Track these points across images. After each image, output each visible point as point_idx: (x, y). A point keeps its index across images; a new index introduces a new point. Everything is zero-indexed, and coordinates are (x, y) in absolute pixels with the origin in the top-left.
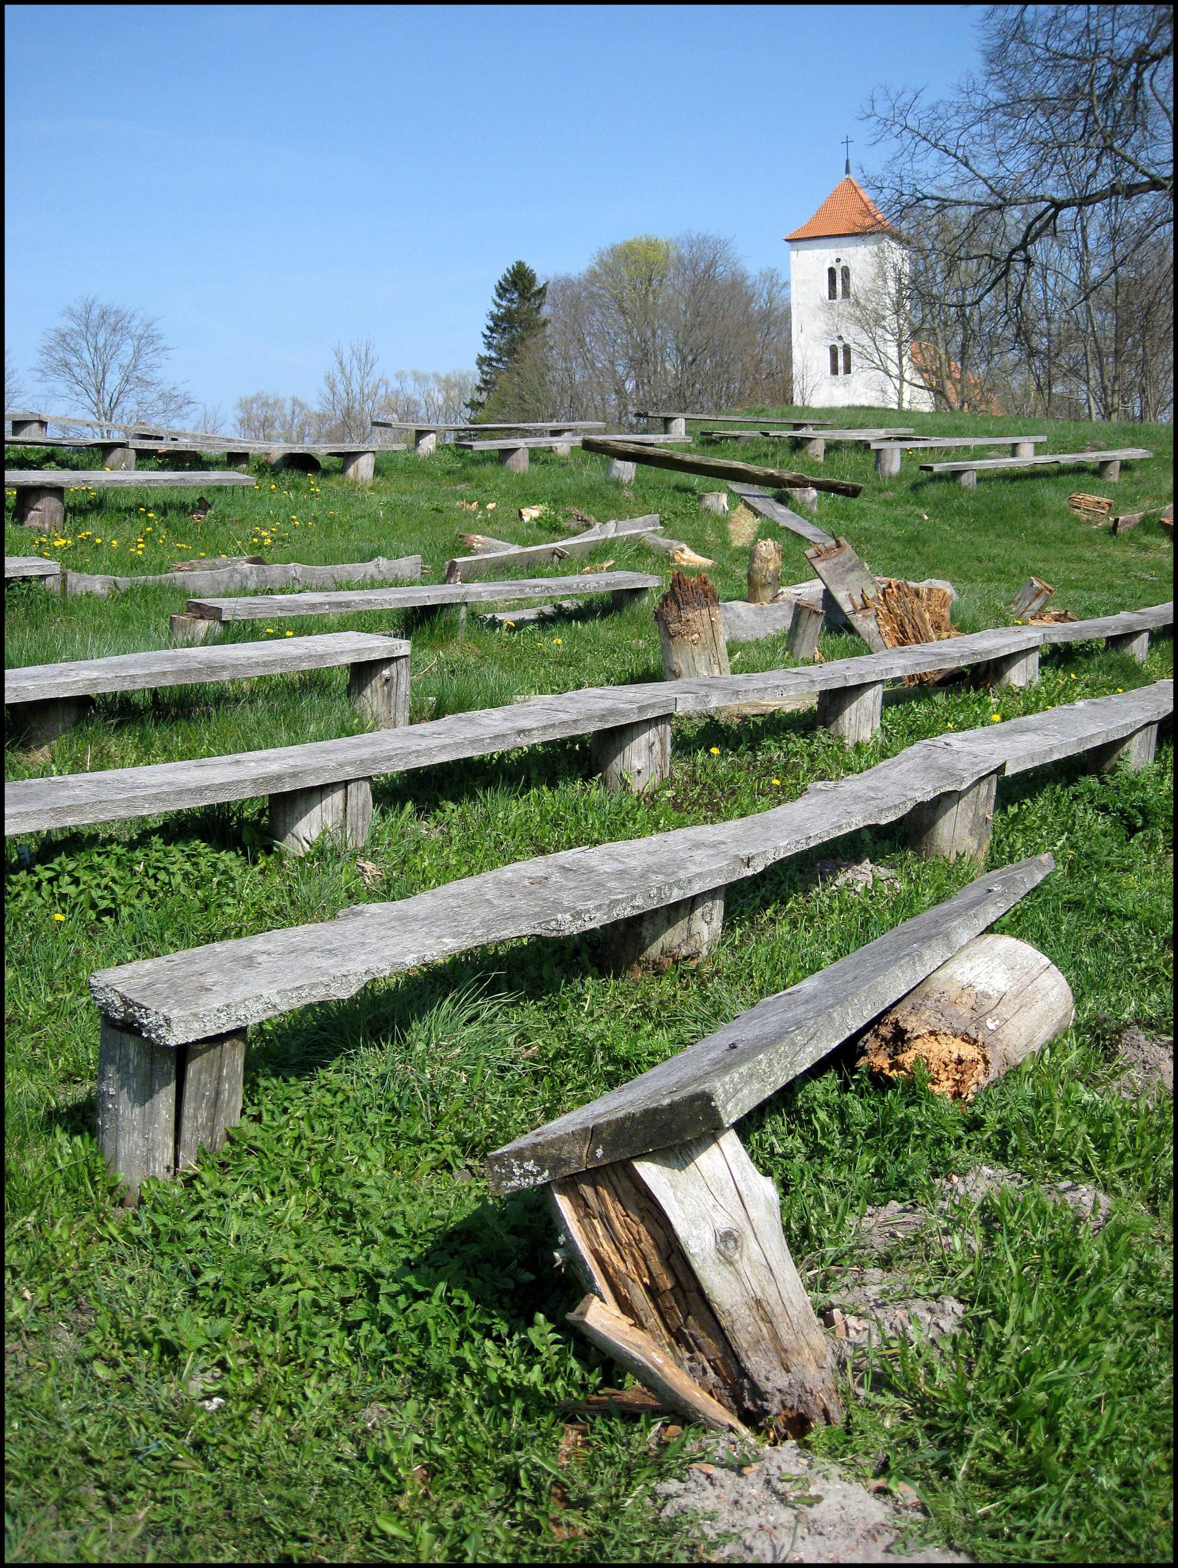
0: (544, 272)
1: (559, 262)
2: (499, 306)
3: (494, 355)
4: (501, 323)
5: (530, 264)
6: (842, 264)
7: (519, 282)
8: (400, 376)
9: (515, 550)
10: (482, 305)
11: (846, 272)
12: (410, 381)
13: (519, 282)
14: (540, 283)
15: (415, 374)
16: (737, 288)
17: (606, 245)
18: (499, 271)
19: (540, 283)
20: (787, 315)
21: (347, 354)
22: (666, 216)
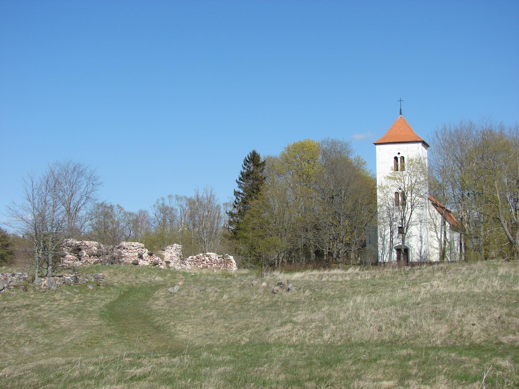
0: (263, 155)
1: (270, 150)
2: (244, 168)
3: (241, 191)
4: (246, 176)
5: (258, 152)
6: (400, 155)
7: (254, 159)
8: (170, 196)
9: (485, 377)
10: (237, 168)
11: (403, 158)
12: (174, 199)
13: (254, 159)
14: (262, 160)
15: (176, 196)
16: (348, 165)
17: (291, 143)
18: (246, 153)
19: (262, 160)
20: (376, 179)
21: (238, 180)
22: (317, 128)
